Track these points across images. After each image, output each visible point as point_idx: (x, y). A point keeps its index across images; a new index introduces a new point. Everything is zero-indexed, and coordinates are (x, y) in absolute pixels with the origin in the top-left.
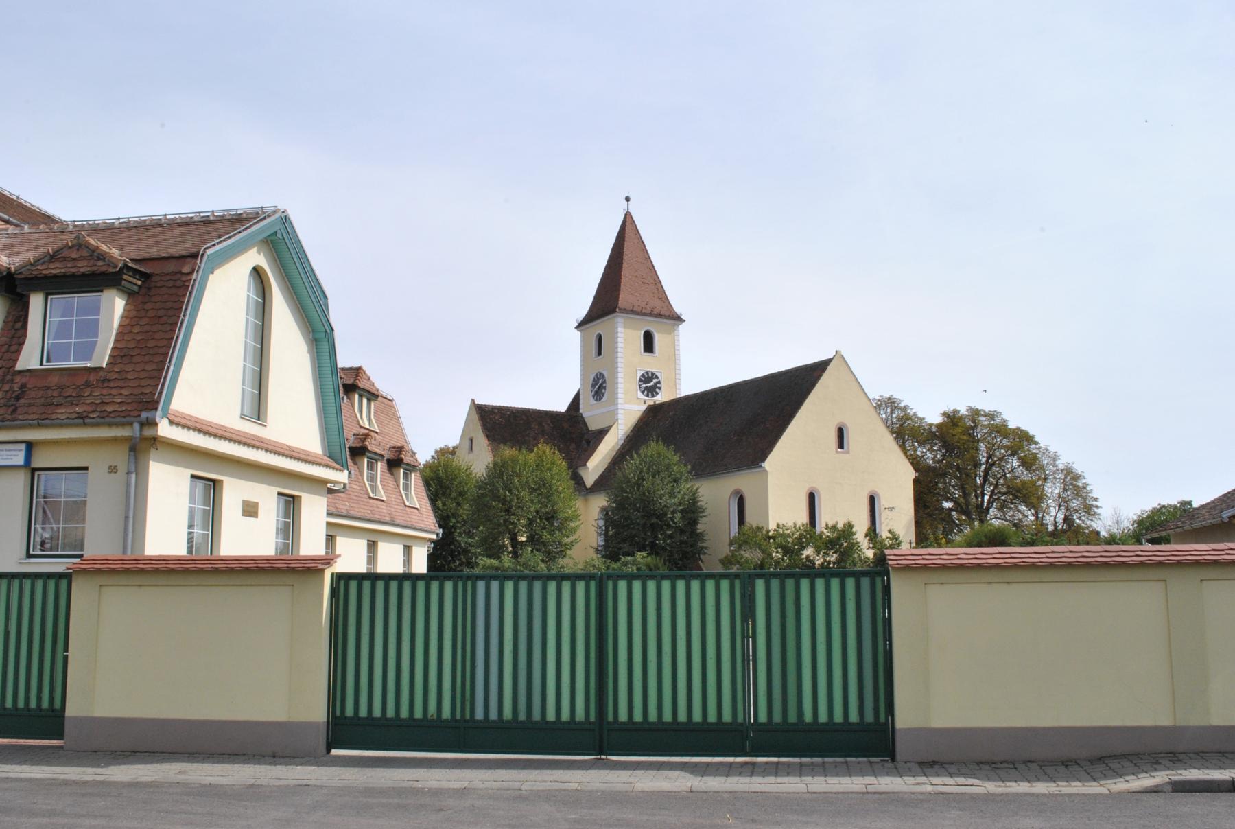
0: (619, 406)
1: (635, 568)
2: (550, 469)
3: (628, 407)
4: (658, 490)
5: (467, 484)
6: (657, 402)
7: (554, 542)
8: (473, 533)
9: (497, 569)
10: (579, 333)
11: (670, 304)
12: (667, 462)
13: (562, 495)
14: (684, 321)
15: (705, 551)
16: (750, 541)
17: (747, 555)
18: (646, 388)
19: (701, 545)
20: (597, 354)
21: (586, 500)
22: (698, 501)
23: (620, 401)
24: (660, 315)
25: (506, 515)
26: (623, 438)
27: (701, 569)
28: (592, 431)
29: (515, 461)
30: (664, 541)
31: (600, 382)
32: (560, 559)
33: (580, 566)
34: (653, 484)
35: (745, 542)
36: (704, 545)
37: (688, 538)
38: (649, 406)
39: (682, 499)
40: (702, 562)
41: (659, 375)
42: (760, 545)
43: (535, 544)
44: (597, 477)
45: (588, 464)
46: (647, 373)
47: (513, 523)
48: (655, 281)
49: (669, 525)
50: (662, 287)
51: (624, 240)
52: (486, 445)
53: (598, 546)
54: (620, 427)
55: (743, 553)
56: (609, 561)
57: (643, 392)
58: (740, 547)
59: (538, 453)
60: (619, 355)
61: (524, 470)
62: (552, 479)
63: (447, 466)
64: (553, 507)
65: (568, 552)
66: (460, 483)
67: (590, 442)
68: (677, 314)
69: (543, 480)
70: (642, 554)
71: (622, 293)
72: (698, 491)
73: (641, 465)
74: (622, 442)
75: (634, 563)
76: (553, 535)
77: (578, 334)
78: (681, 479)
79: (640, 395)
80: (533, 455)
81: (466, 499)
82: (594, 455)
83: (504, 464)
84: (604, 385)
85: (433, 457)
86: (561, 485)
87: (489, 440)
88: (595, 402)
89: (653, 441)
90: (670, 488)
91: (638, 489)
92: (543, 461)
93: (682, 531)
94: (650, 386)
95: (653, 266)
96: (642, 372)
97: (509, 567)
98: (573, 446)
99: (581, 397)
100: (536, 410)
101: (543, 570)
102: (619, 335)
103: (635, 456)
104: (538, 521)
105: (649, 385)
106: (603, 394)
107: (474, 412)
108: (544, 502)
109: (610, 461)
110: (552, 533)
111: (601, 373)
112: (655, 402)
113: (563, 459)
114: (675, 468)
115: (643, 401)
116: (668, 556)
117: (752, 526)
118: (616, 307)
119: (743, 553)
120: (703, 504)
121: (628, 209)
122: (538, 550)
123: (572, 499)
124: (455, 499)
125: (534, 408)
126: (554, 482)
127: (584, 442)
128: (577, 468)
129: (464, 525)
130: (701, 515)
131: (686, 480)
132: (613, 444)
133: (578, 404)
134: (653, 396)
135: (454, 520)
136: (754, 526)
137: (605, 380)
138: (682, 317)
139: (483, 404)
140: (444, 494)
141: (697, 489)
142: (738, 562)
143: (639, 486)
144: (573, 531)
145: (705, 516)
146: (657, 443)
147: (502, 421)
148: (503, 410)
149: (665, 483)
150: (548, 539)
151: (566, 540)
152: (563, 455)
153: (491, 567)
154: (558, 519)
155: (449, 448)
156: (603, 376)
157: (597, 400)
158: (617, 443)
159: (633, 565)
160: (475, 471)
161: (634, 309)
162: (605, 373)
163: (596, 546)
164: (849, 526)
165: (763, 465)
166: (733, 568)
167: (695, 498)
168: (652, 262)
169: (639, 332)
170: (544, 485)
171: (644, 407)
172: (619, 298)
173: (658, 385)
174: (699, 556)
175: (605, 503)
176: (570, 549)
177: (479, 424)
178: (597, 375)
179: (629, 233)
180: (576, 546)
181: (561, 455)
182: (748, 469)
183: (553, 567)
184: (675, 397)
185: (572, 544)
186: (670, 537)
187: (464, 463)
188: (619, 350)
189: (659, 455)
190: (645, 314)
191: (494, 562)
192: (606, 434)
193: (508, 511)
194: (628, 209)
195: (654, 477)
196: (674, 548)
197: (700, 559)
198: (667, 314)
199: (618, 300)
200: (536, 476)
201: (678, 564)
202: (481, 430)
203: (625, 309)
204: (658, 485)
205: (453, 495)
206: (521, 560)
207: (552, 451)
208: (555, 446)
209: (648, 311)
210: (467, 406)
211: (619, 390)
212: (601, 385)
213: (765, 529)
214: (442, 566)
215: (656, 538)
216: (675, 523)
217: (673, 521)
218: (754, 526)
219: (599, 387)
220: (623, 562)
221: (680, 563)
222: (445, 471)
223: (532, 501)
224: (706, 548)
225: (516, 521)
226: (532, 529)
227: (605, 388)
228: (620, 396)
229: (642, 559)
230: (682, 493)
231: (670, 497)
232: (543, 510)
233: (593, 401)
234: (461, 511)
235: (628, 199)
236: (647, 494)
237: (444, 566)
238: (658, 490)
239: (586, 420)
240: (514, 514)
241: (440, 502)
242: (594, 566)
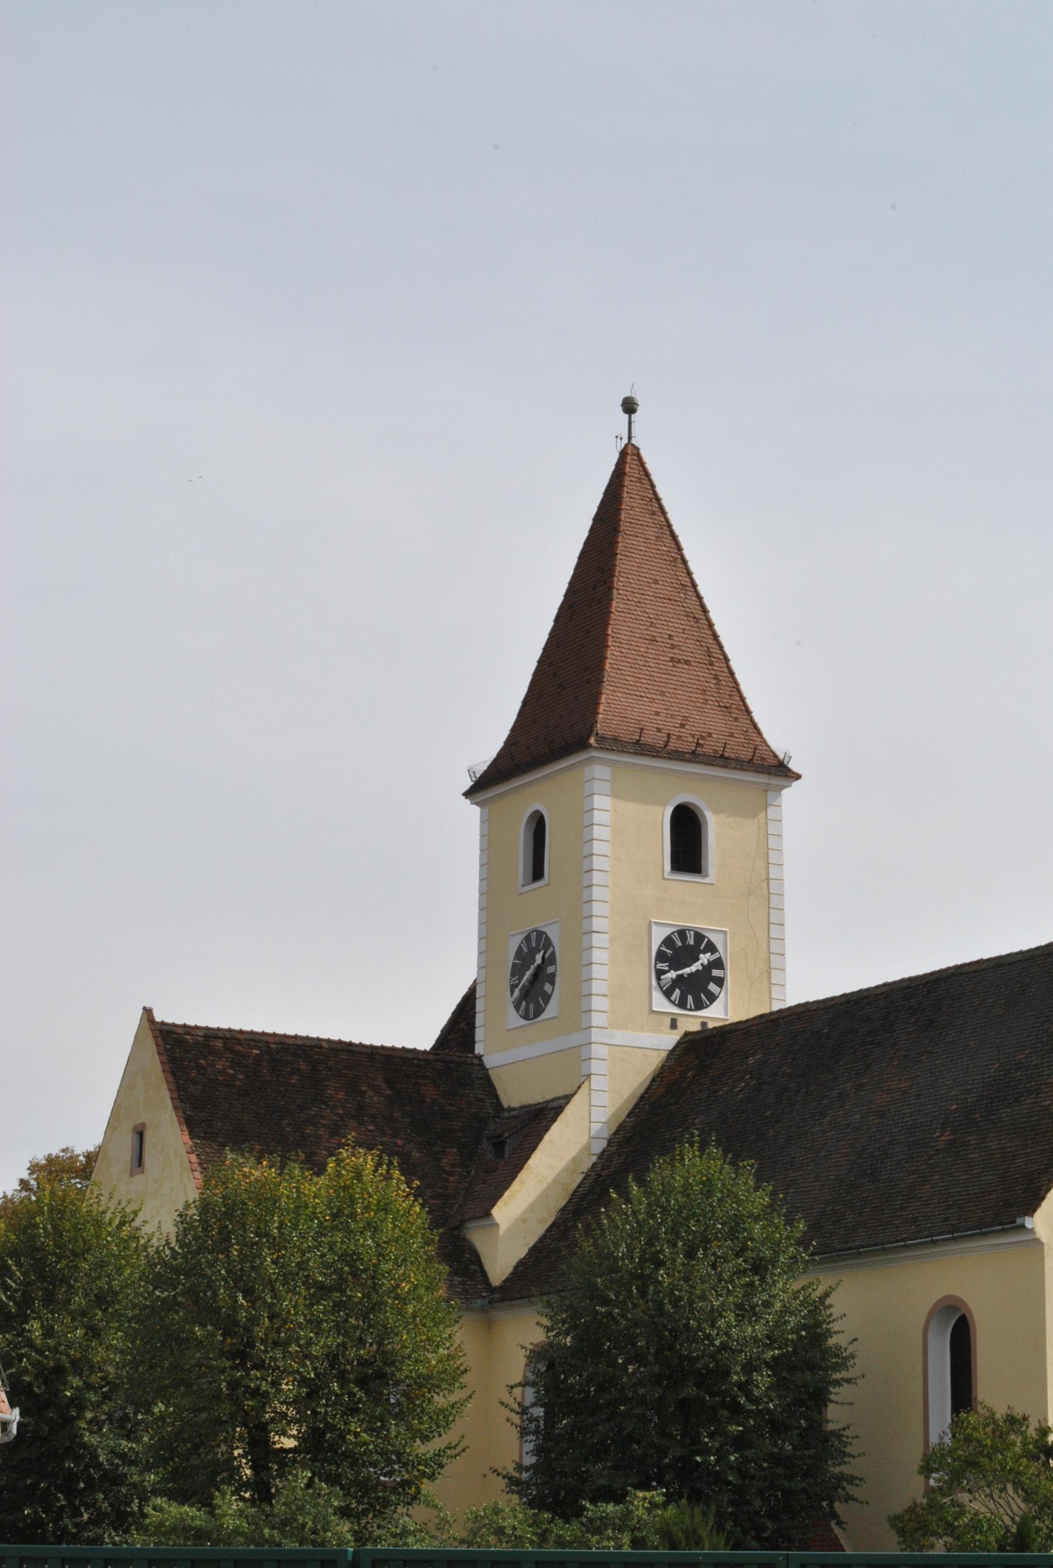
0: (596, 1035)
1: (626, 1539)
2: (374, 1228)
3: (620, 1037)
4: (703, 1297)
5: (119, 1270)
6: (711, 1025)
7: (383, 1453)
8: (138, 1423)
9: (200, 1535)
10: (476, 810)
11: (755, 726)
12: (730, 1208)
13: (410, 1309)
14: (798, 777)
15: (851, 1490)
16: (984, 1461)
17: (976, 1506)
18: (679, 981)
19: (837, 1470)
20: (530, 875)
21: (489, 1324)
22: (829, 1333)
23: (596, 1019)
24: (722, 756)
25: (235, 1368)
26: (606, 1135)
27: (837, 1545)
28: (510, 1109)
29: (267, 1201)
30: (722, 1457)
31: (538, 959)
32: (400, 1509)
33: (459, 1532)
34: (686, 1279)
35: (971, 1463)
36: (845, 1469)
37: (795, 1448)
38: (687, 1034)
39: (777, 1325)
40: (840, 1523)
41: (716, 940)
42: (1019, 1473)
43: (325, 1460)
44: (522, 1253)
45: (495, 1212)
46: (682, 933)
47: (255, 1393)
48: (709, 654)
49: (735, 1409)
50: (732, 673)
51: (616, 530)
52: (183, 1150)
53: (520, 1467)
54: (597, 1099)
55: (964, 1497)
56: (547, 1516)
57: (668, 994)
58: (955, 1479)
59: (339, 1175)
60: (597, 878)
61: (295, 1227)
62: (381, 1255)
63: (62, 1212)
64: (380, 1344)
65: (426, 1486)
66: (102, 1264)
67: (503, 1143)
68: (775, 756)
69: (350, 1258)
70: (648, 1494)
71: (606, 689)
72: (828, 1302)
73: (654, 1217)
74: (600, 1146)
75: (623, 1523)
76: (378, 1431)
77: (472, 813)
78: (774, 1262)
79: (661, 1003)
80: (322, 1180)
81: (117, 1315)
82: (515, 1185)
83: (232, 1210)
84: (550, 970)
85: (23, 1182)
86: (405, 1277)
87: (192, 1135)
88: (523, 1022)
89: (691, 1144)
90: (740, 1292)
91: (643, 1294)
92: (353, 1201)
93: (777, 1427)
94: (690, 975)
95: (705, 611)
96: (668, 931)
97: (237, 1532)
98: (450, 1158)
99: (480, 1005)
100: (340, 1042)
101: (341, 1542)
102: (597, 816)
103: (635, 1188)
104: (335, 1386)
105: (687, 970)
106: (547, 998)
107: (150, 1047)
108: (356, 1327)
109: (562, 1203)
110: (376, 1426)
111: (540, 934)
112: (704, 1024)
113: (416, 1197)
114: (757, 1227)
115: (667, 1021)
116: (731, 1502)
117: (993, 1414)
118: (590, 730)
119: (964, 1497)
120: (844, 1345)
121: (630, 437)
122: (332, 1480)
123: (442, 1321)
124: (83, 1314)
125: (335, 1037)
126: (385, 1267)
127: (485, 1144)
128: (461, 1226)
129: (106, 1397)
130: (837, 1376)
131: (790, 1270)
132: (573, 1151)
133: (472, 1026)
134: (699, 1006)
135: (76, 1382)
136: (1000, 1413)
137: (553, 954)
138: (793, 766)
139: (180, 1021)
140: (49, 1299)
141: (826, 1295)
142: (950, 1529)
143: (644, 1281)
144: (443, 1419)
145: (848, 1381)
146: (702, 1150)
147: (234, 1077)
148: (239, 1042)
149: (725, 1276)
150: (366, 1444)
151: (422, 1449)
152: (417, 1183)
153: (181, 1529)
154: (397, 1383)
155: (74, 1158)
156: (548, 943)
157: (526, 1017)
158: (587, 1148)
159: (621, 1530)
160: (147, 1230)
161: (643, 740)
162: (553, 933)
163: (510, 1469)
164: (1025, 1418)
165: (1029, 1222)
166: (932, 1546)
167: (818, 1325)
168: (700, 598)
169: (659, 810)
170: (355, 1274)
171: (669, 1040)
172: (597, 704)
173: (716, 973)
174: (831, 1505)
175: (539, 1336)
176: (432, 1477)
177: (165, 1086)
178: (528, 938)
179: (630, 488)
180: (452, 1467)
181: (409, 1183)
182: (983, 1234)
183: (377, 1532)
184: (765, 1010)
185: (436, 1464)
186: (740, 1443)
187: (112, 1205)
188: (597, 863)
189: (708, 1187)
190: (677, 756)
191: (190, 1512)
192: (554, 1120)
193: (242, 1355)
194: (630, 437)
195: (690, 1255)
196: (753, 1477)
197: (834, 1515)
198: (746, 754)
199: (596, 713)
200: (331, 1246)
201: (765, 1529)
202: (169, 1104)
203: (615, 740)
204: (703, 1282)
205: (79, 1301)
206: (279, 1507)
207: (383, 1170)
208: (390, 1155)
209: (688, 746)
210: (131, 1024)
211: (597, 987)
212: (540, 969)
213: (1033, 1424)
214: (37, 1523)
215: (695, 1445)
216: (756, 1401)
217: (749, 1395)
218: (1000, 1413)
219: (536, 976)
220: (591, 1520)
221: (771, 1526)
222: (54, 1227)
223: (315, 1325)
224: (851, 1480)
225: (264, 1387)
226: (315, 1413)
227: (552, 979)
228: (597, 1003)
229: (649, 1511)
230: (778, 1305)
231: (740, 1318)
232: (352, 1353)
233: (515, 1019)
234: (98, 1355)
235: (629, 407)
236: (669, 1308)
237: (42, 1524)
238: (703, 1297)
239: (492, 1074)
240: (260, 1366)
241: (36, 1325)
242: (500, 1531)
